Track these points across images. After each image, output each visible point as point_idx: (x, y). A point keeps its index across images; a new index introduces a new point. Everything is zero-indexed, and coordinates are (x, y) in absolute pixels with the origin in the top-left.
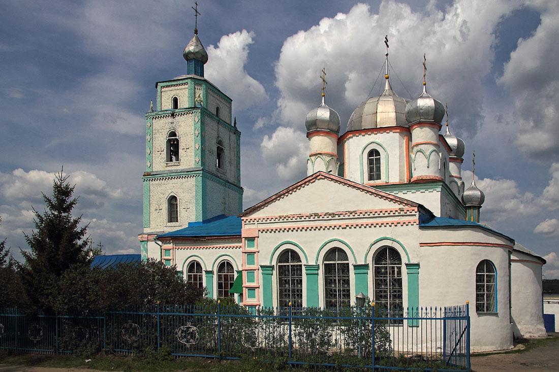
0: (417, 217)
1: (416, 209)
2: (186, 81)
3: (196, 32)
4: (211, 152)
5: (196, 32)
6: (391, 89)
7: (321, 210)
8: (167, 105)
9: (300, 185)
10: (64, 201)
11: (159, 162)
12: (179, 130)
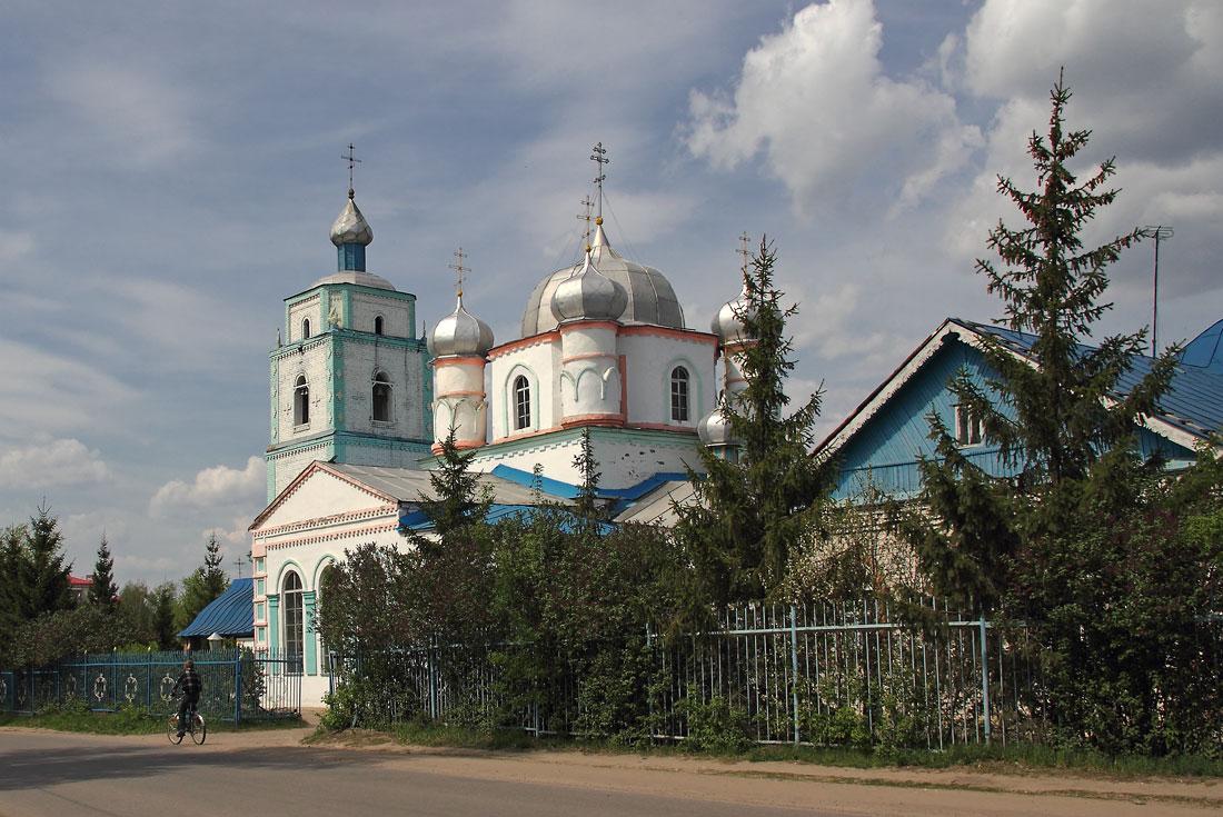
0: (397, 518)
1: (396, 506)
2: (318, 291)
3: (352, 195)
4: (359, 398)
5: (352, 195)
6: (608, 244)
7: (315, 516)
8: (297, 334)
9: (307, 475)
10: (45, 537)
11: (285, 427)
12: (308, 372)
